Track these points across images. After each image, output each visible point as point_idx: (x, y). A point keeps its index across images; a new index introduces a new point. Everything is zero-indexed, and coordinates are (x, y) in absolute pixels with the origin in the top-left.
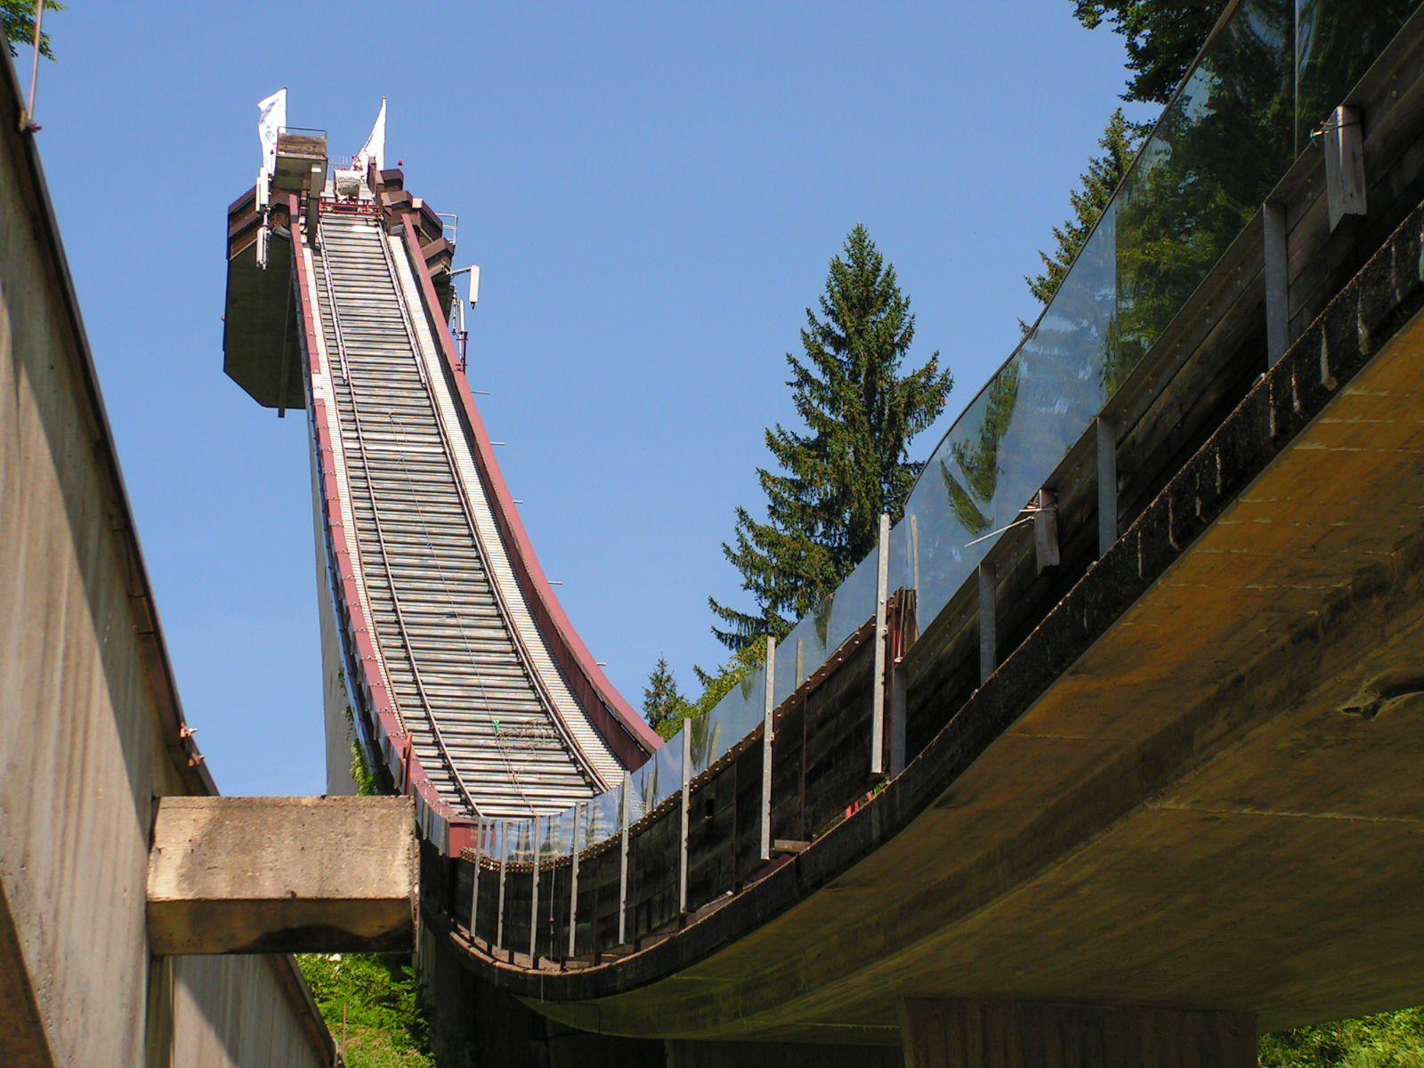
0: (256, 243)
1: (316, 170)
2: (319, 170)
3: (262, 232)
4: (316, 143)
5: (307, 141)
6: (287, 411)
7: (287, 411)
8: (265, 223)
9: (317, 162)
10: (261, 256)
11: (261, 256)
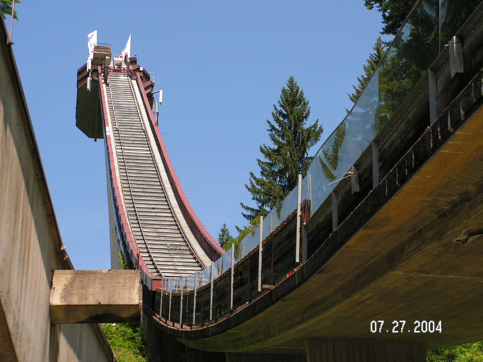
0: (87, 82)
1: (107, 57)
2: (108, 58)
3: (89, 79)
4: (107, 49)
5: (104, 48)
6: (97, 139)
7: (97, 139)
8: (90, 76)
9: (108, 55)
10: (88, 87)
11: (88, 87)
